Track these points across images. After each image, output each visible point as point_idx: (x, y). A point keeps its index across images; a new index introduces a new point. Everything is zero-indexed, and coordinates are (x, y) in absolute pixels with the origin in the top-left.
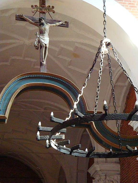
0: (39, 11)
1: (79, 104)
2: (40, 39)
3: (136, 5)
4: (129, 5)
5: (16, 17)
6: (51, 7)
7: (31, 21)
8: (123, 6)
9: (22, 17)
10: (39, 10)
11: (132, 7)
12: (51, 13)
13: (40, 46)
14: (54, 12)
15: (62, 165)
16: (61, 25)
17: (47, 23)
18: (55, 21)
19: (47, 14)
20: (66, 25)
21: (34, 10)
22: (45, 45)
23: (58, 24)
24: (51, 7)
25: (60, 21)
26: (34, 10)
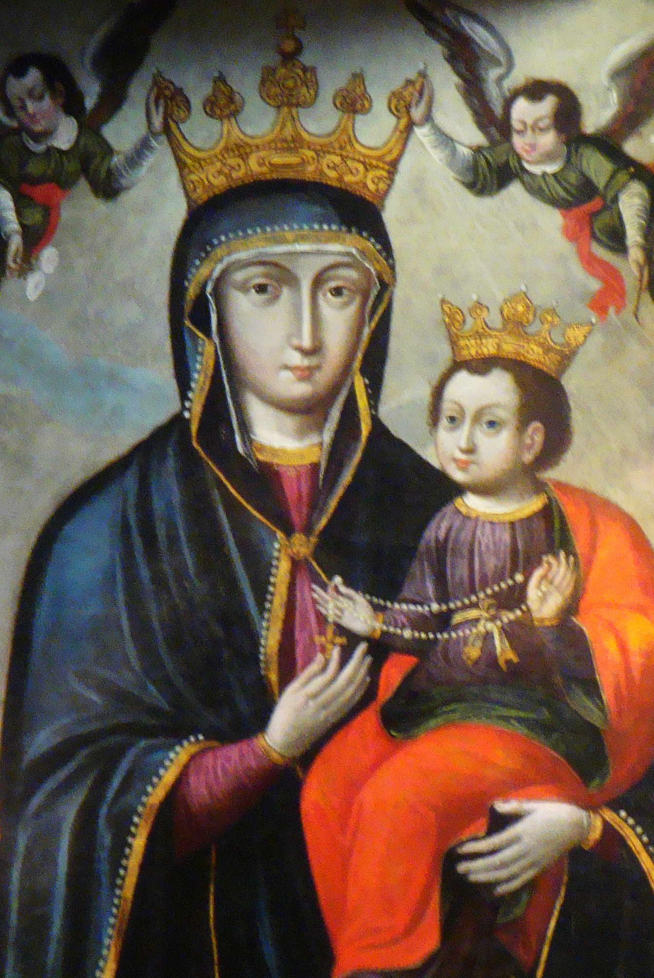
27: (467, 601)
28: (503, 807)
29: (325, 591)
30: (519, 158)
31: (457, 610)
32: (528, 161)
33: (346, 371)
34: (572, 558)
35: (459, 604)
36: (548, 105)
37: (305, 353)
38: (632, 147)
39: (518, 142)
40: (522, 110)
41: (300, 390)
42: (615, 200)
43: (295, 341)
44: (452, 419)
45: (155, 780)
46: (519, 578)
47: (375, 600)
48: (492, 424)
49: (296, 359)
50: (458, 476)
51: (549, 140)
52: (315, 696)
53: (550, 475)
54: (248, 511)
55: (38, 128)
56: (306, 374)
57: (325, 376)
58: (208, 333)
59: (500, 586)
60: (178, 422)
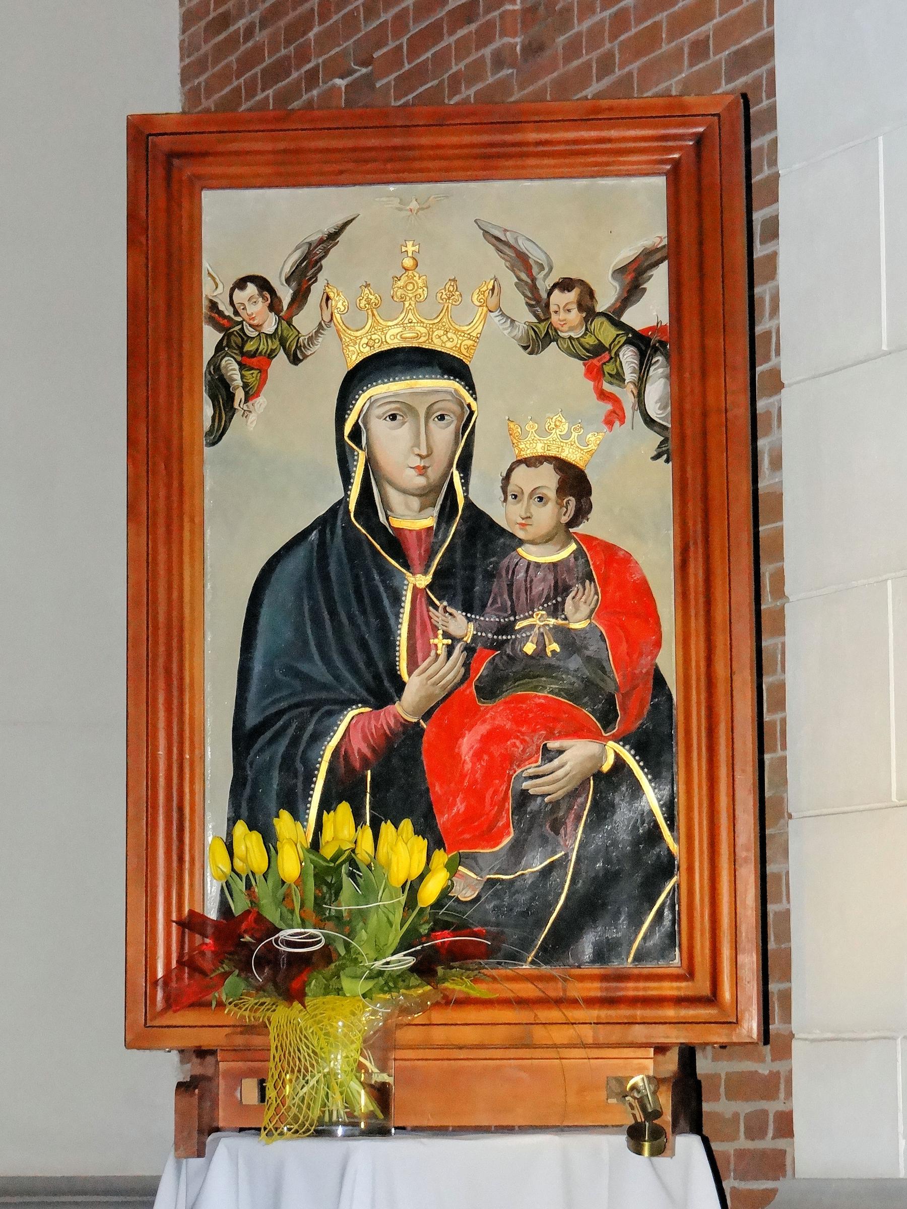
27: (527, 614)
28: (553, 745)
29: (437, 610)
30: (556, 330)
31: (519, 620)
32: (561, 331)
33: (447, 473)
34: (593, 583)
35: (522, 616)
36: (572, 296)
37: (421, 457)
38: (625, 319)
39: (554, 318)
40: (559, 299)
41: (421, 481)
42: (617, 354)
43: (417, 451)
44: (516, 496)
45: (406, 582)
46: (559, 599)
47: (469, 615)
48: (541, 499)
49: (417, 462)
50: (520, 534)
51: (575, 316)
52: (430, 678)
53: (582, 529)
54: (387, 560)
55: (255, 322)
56: (422, 471)
57: (434, 474)
58: (361, 448)
59: (223, 968)
60: (343, 503)
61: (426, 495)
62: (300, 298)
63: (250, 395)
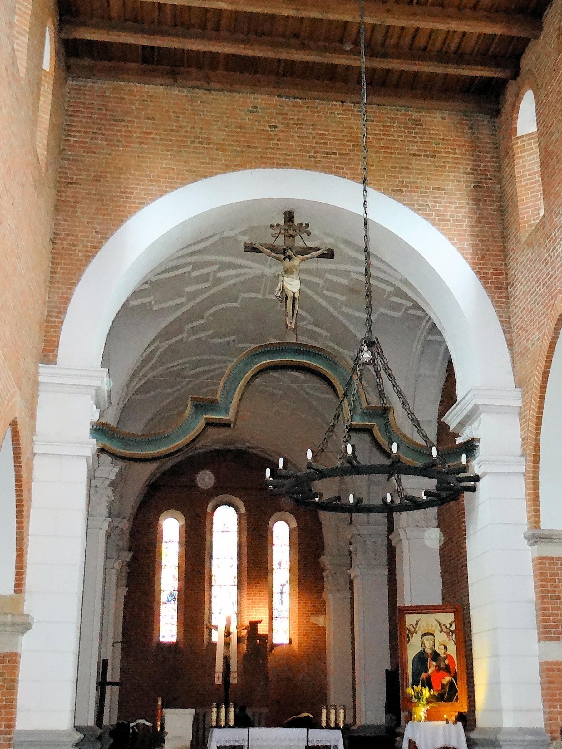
0: (282, 234)
1: (275, 463)
2: (285, 284)
3: (448, 218)
4: (437, 218)
5: (246, 247)
6: (304, 225)
7: (412, 461)
8: (427, 219)
9: (255, 247)
10: (283, 232)
11: (443, 220)
12: (304, 236)
13: (284, 297)
14: (309, 234)
15: (468, 95)
16: (322, 256)
17: (296, 254)
18: (311, 248)
19: (298, 238)
20: (330, 254)
21: (275, 232)
22: (294, 293)
23: (315, 253)
24: (304, 225)
25: (318, 249)
26: (275, 232)
61: (430, 649)
62: (416, 627)
63: (412, 637)
